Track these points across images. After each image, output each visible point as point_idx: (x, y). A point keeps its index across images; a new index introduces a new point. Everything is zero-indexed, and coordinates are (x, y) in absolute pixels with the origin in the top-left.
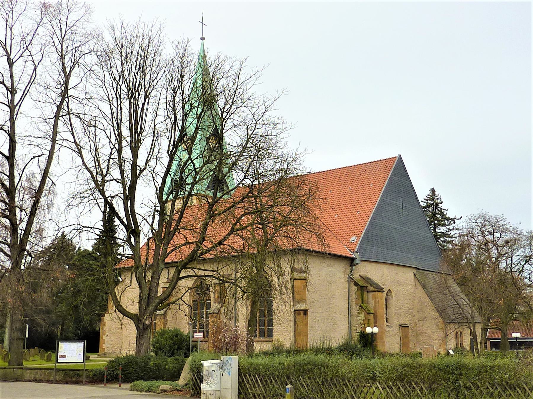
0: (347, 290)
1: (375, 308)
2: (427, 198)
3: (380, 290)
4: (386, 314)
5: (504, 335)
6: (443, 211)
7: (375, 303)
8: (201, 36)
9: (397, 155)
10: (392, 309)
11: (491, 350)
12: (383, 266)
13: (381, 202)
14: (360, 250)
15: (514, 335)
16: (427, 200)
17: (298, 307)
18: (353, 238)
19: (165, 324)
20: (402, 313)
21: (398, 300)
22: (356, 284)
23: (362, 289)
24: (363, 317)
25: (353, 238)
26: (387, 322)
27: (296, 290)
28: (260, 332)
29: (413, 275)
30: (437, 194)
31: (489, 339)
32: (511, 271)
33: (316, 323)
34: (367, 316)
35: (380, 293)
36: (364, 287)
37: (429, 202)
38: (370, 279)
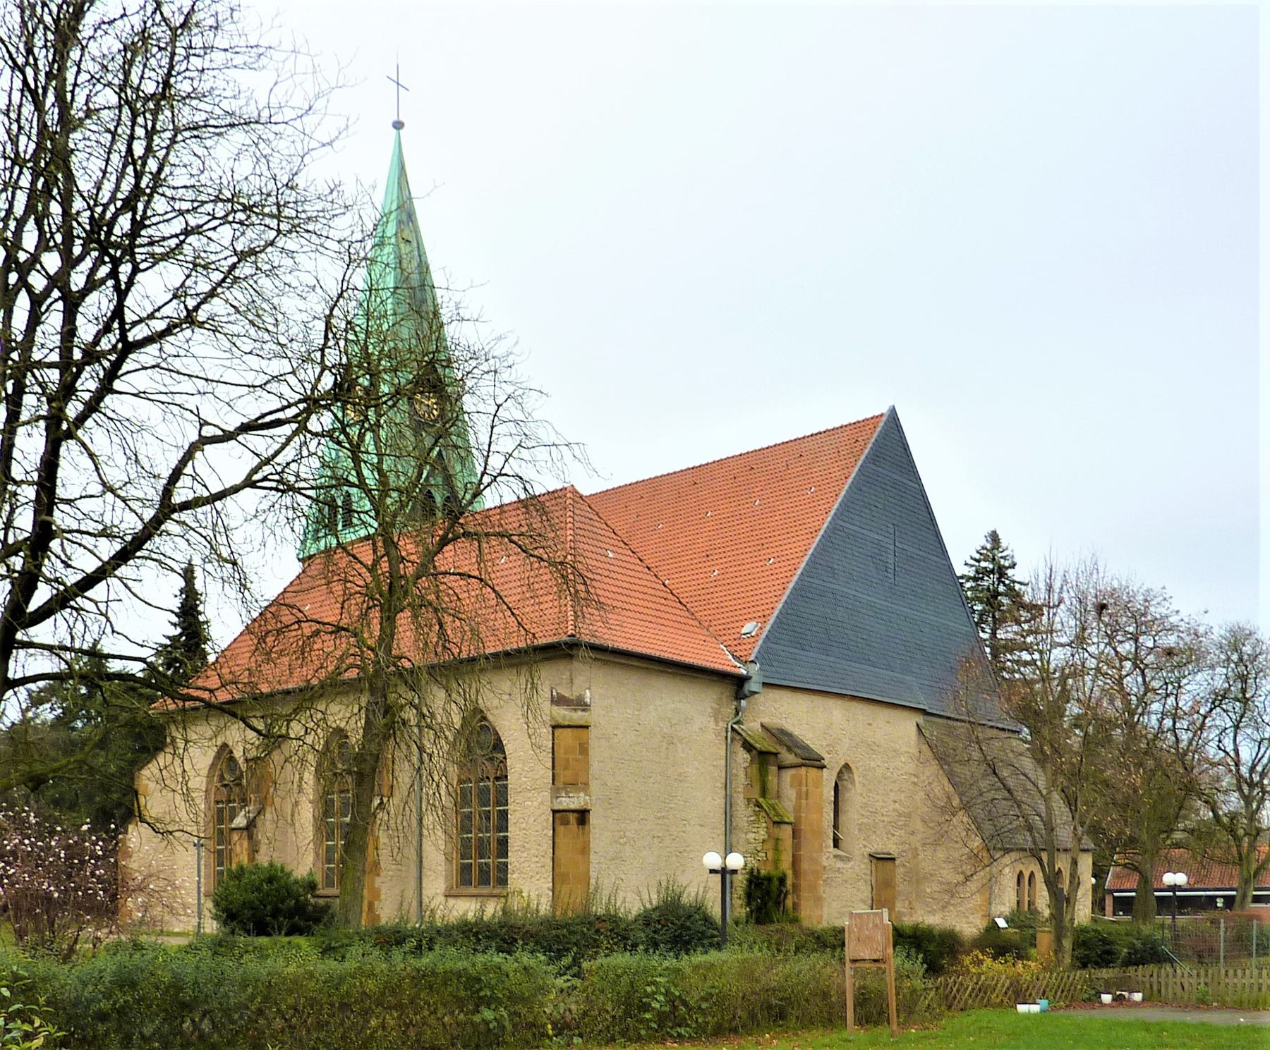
0: (723, 762)
1: (798, 809)
2: (978, 556)
3: (814, 761)
4: (836, 827)
5: (1145, 880)
6: (1017, 587)
7: (799, 796)
8: (395, 119)
9: (884, 409)
10: (851, 816)
11: (1114, 914)
12: (831, 703)
13: (833, 530)
14: (765, 657)
15: (1169, 878)
16: (978, 561)
17: (567, 802)
18: (749, 627)
19: (254, 851)
20: (881, 825)
21: (870, 791)
22: (748, 746)
23: (763, 758)
24: (762, 834)
25: (749, 627)
26: (836, 845)
27: (560, 753)
28: (750, 882)
29: (915, 728)
30: (1004, 544)
31: (1111, 892)
32: (1174, 730)
33: (627, 847)
34: (775, 830)
35: (813, 772)
36: (769, 757)
37: (983, 564)
38: (790, 735)
